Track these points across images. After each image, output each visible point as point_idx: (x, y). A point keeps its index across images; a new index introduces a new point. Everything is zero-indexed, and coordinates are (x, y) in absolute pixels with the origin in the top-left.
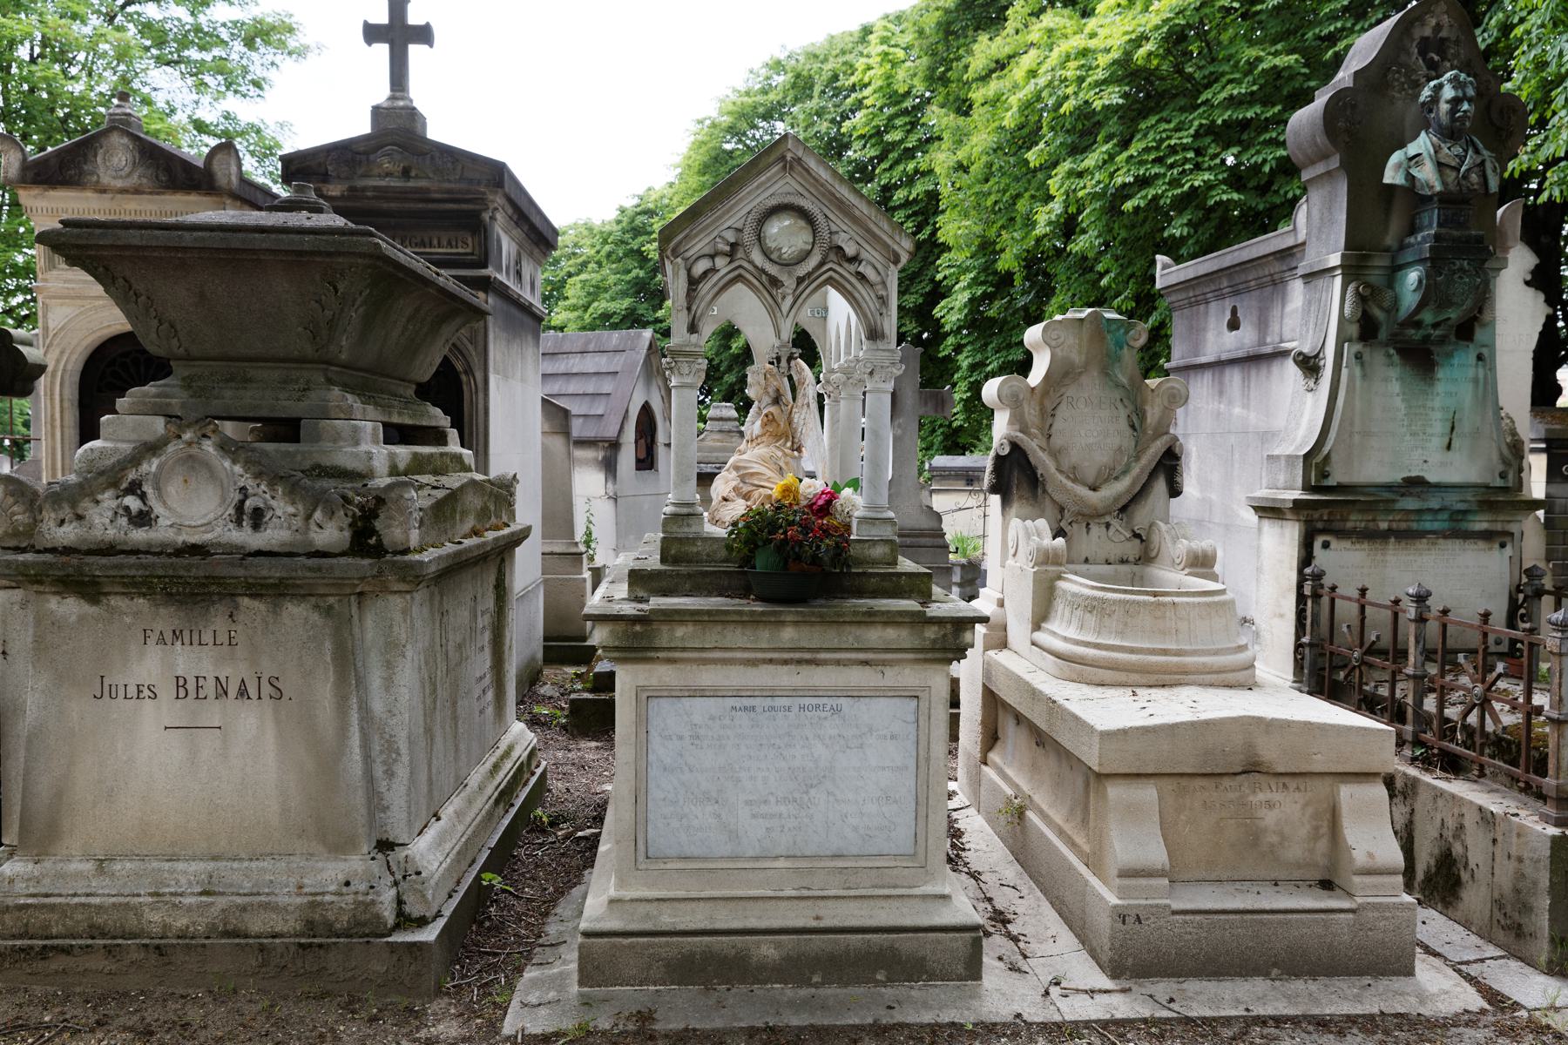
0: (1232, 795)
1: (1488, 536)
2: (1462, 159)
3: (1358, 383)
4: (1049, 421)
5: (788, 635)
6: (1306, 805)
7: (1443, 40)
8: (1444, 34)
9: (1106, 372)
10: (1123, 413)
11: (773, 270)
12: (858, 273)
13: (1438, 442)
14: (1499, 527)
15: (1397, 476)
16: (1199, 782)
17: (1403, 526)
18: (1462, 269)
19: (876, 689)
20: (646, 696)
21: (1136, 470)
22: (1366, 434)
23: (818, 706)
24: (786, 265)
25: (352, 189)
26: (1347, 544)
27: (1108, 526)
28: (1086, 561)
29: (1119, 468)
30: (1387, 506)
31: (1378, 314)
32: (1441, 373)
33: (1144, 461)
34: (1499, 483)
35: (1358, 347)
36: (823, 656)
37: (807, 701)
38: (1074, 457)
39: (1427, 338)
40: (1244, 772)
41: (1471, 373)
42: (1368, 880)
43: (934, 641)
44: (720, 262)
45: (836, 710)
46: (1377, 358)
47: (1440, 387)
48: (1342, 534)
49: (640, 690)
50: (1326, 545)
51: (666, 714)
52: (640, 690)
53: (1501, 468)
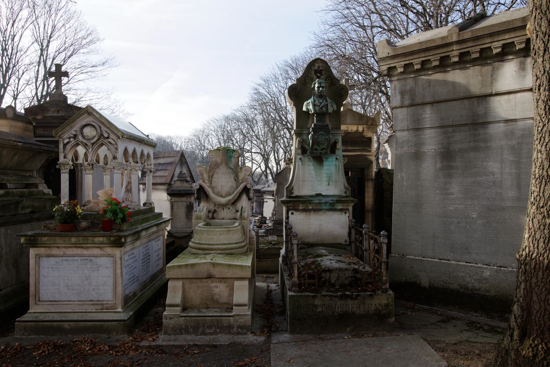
0: (205, 284)
1: (341, 210)
2: (321, 103)
3: (301, 166)
4: (211, 179)
5: (73, 240)
6: (227, 287)
7: (321, 70)
8: (321, 68)
9: (227, 165)
10: (232, 176)
11: (85, 141)
12: (109, 142)
13: (325, 183)
14: (345, 208)
15: (314, 193)
16: (195, 281)
17: (316, 207)
18: (321, 134)
19: (101, 255)
20: (38, 257)
21: (235, 193)
22: (304, 181)
23: (85, 260)
24: (89, 140)
25: (44, 117)
26: (299, 213)
27: (229, 209)
28: (223, 219)
29: (231, 192)
30: (310, 202)
31: (306, 146)
32: (325, 163)
33: (238, 190)
34: (344, 195)
35: (300, 156)
36: (83, 245)
37: (83, 258)
38: (219, 189)
39: (321, 153)
40: (206, 278)
41: (334, 163)
42: (237, 308)
43: (113, 241)
44: (72, 140)
45: (91, 261)
46: (306, 159)
47: (325, 167)
48: (297, 210)
49: (36, 255)
50: (292, 213)
51: (45, 262)
52: (36, 255)
53: (345, 190)
